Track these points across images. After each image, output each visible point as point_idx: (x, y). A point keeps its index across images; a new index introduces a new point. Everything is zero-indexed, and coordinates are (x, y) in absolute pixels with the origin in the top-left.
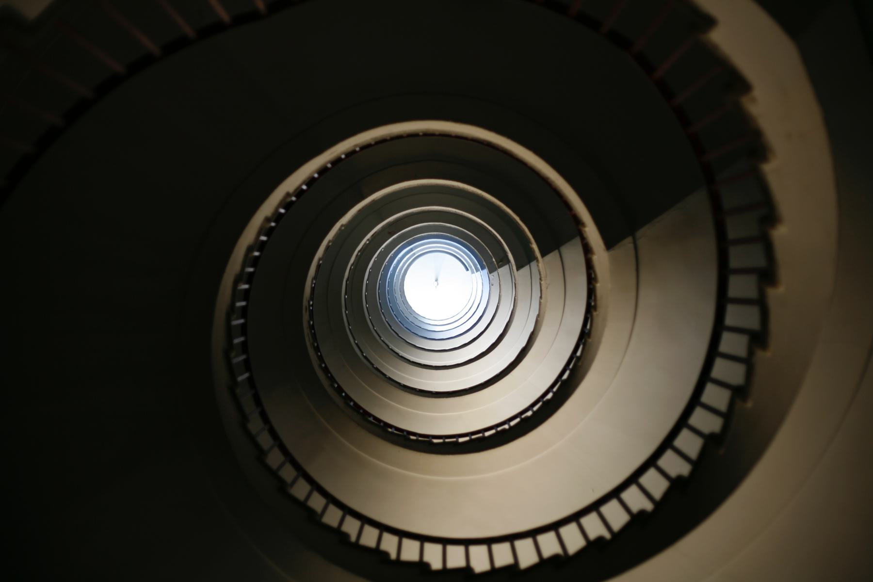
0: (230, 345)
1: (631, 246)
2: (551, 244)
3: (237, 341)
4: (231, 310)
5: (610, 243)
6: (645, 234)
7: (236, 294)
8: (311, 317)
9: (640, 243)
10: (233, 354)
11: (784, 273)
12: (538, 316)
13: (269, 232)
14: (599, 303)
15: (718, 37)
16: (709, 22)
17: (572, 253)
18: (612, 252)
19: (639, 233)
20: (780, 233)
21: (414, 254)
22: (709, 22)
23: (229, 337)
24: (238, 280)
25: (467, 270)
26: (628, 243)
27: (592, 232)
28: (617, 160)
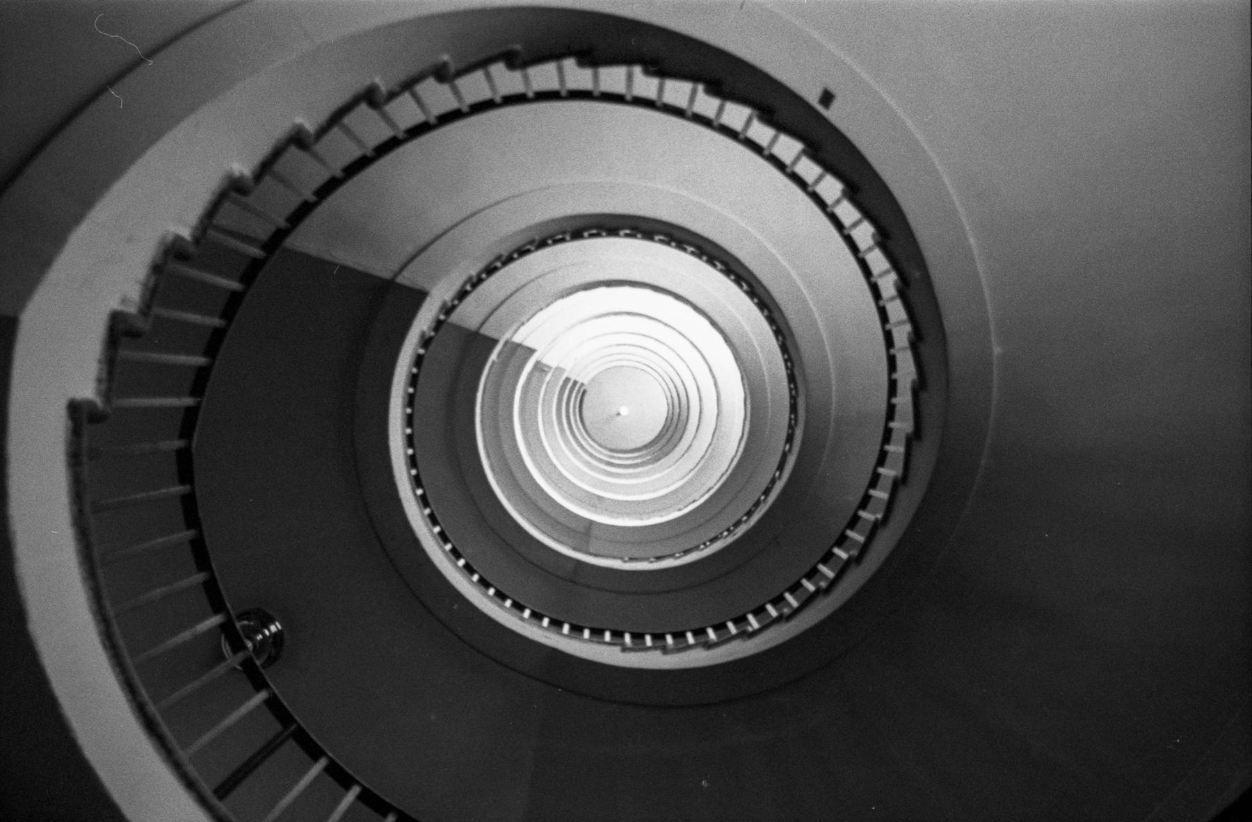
0: (780, 619)
1: (405, 273)
2: (476, 345)
3: (811, 587)
4: (745, 635)
5: (419, 296)
6: (381, 268)
7: (725, 639)
8: (738, 524)
9: (395, 267)
10: (750, 629)
11: (280, 130)
12: (562, 297)
13: (638, 637)
14: (491, 258)
15: (87, 390)
16: (75, 409)
17: (469, 314)
18: (426, 286)
19: (387, 275)
20: (242, 167)
21: (587, 464)
22: (75, 409)
23: (812, 597)
24: (709, 646)
25: (584, 392)
26: (405, 279)
27: (423, 322)
28: (298, 369)
